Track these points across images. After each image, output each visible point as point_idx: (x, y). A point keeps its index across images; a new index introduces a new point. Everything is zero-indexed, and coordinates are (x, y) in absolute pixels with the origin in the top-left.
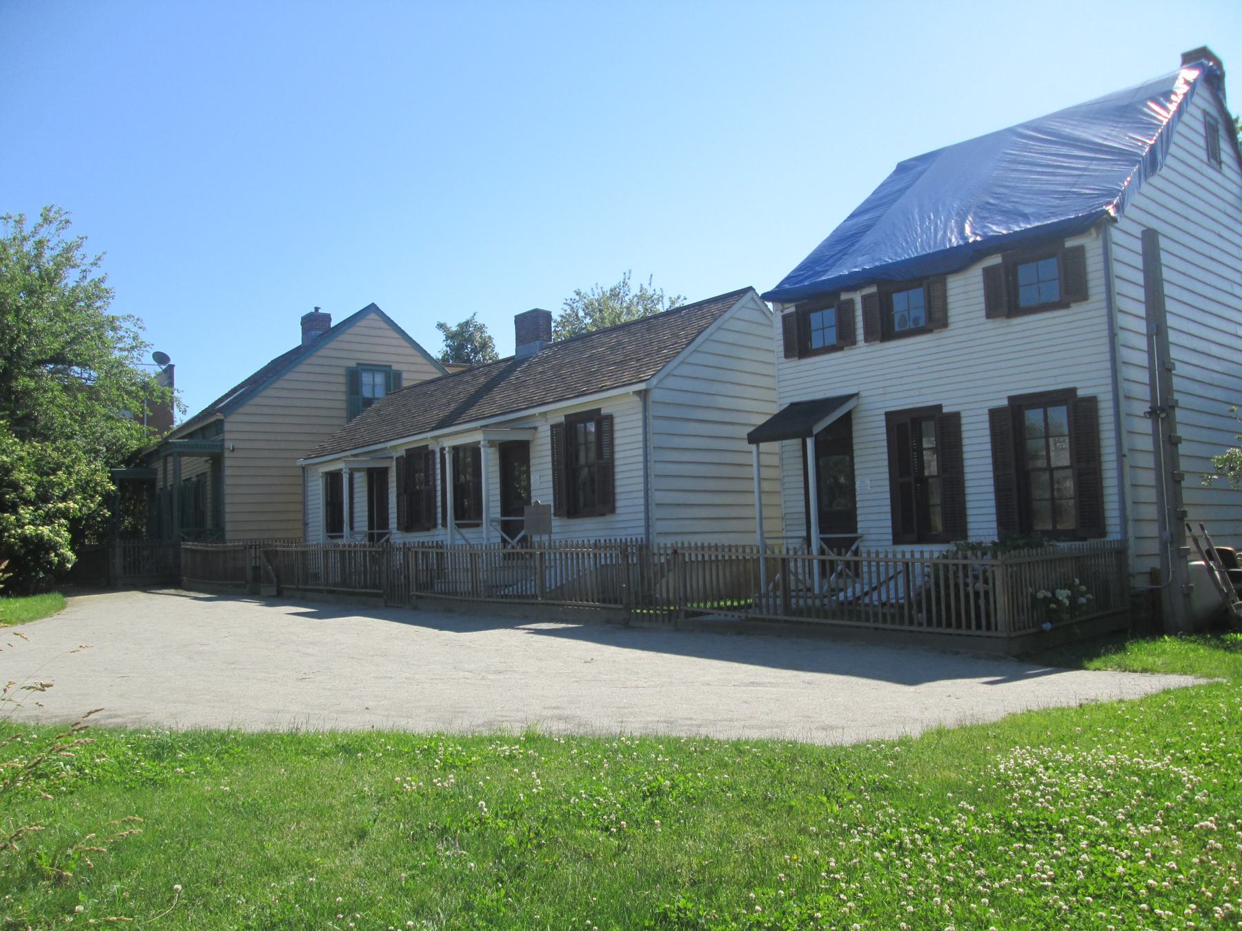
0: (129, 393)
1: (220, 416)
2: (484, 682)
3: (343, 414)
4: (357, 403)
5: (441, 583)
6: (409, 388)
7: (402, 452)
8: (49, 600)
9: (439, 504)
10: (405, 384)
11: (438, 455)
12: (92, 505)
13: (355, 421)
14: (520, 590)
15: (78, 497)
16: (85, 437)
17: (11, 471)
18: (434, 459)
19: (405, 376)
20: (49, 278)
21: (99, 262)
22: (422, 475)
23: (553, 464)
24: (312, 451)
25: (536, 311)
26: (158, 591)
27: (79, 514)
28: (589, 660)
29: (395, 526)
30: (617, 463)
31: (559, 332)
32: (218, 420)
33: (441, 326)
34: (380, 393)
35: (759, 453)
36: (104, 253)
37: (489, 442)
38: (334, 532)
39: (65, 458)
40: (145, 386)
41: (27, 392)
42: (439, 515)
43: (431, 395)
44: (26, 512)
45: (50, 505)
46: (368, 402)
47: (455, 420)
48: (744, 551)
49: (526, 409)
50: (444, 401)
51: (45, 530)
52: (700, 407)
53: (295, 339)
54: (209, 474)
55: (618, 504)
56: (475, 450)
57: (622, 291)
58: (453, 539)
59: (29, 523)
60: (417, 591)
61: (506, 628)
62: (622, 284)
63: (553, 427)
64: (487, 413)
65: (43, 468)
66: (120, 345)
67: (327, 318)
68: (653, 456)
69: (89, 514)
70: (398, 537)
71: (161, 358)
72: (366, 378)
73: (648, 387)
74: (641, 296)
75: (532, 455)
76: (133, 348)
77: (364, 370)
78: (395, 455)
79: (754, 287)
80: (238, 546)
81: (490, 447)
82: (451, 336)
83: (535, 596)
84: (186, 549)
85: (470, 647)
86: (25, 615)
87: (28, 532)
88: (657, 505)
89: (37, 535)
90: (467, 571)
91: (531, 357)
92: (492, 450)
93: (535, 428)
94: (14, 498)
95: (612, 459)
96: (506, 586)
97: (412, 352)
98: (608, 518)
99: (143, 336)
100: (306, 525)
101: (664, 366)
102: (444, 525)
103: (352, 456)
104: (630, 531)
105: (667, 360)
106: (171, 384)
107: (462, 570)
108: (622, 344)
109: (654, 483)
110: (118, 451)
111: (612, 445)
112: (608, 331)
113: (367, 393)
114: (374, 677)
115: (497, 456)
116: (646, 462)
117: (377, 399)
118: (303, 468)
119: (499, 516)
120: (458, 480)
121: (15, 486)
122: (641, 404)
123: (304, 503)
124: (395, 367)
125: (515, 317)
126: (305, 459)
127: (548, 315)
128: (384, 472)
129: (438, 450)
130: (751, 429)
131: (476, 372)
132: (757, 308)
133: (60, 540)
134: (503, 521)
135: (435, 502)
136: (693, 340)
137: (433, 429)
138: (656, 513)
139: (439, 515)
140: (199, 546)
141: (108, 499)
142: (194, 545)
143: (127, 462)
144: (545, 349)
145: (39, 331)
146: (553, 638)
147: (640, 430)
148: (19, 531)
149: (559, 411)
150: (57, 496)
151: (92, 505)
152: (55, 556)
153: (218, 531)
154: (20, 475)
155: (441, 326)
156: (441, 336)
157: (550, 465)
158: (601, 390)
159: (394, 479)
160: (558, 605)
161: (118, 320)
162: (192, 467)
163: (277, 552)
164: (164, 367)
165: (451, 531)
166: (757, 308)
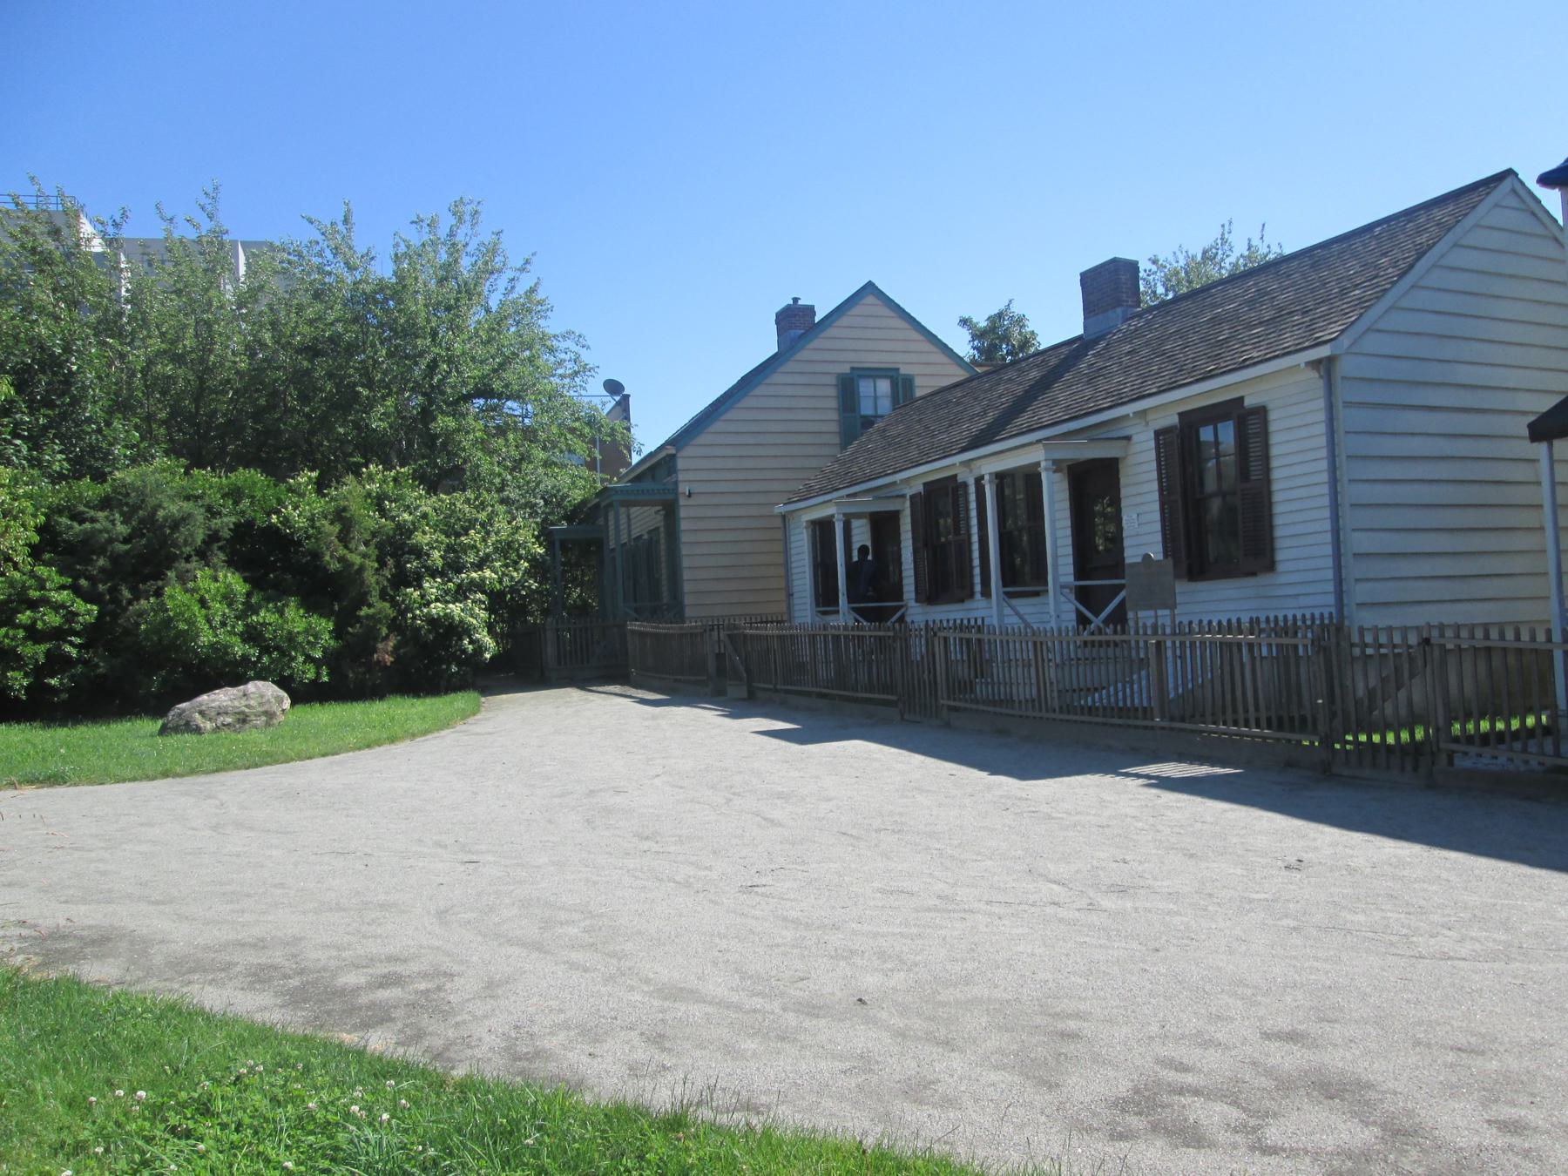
0: (572, 430)
1: (672, 450)
2: (1094, 918)
3: (836, 440)
4: (854, 424)
5: (987, 684)
6: (921, 398)
7: (918, 487)
8: (460, 700)
9: (976, 562)
10: (919, 393)
11: (972, 489)
12: (515, 574)
13: (850, 450)
14: (1112, 699)
15: (498, 564)
16: (519, 487)
17: (412, 532)
18: (966, 494)
19: (918, 382)
20: (469, 291)
21: (528, 267)
22: (949, 521)
23: (1161, 494)
24: (794, 492)
25: (1114, 261)
26: (600, 689)
27: (498, 586)
28: (1292, 860)
29: (913, 595)
30: (1275, 487)
31: (1154, 287)
32: (668, 455)
33: (965, 322)
34: (885, 406)
35: (1552, 461)
36: (534, 254)
37: (1055, 462)
38: (829, 605)
39: (478, 512)
40: (591, 422)
41: (449, 435)
42: (977, 579)
43: (958, 404)
44: (431, 587)
45: (463, 575)
46: (868, 422)
47: (998, 433)
48: (1458, 636)
49: (1110, 408)
50: (978, 409)
51: (455, 609)
52: (1426, 384)
53: (767, 345)
54: (662, 529)
55: (1280, 556)
56: (1031, 478)
57: (1220, 252)
58: (1001, 616)
59: (437, 600)
60: (949, 698)
61: (1106, 772)
62: (1219, 241)
63: (1158, 434)
64: (1046, 420)
65: (453, 527)
66: (560, 371)
67: (810, 310)
68: (1344, 474)
69: (512, 586)
70: (917, 613)
71: (613, 387)
72: (865, 388)
73: (1338, 352)
74: (1249, 257)
75: (1123, 481)
76: (576, 373)
77: (860, 377)
78: (909, 492)
79: (1516, 169)
80: (696, 627)
81: (1055, 472)
82: (978, 335)
83: (1147, 713)
84: (633, 632)
85: (1049, 817)
86: (417, 726)
87: (434, 611)
88: (1356, 555)
89: (446, 614)
90: (1030, 666)
91: (1110, 333)
92: (1058, 476)
93: (1128, 438)
94: (417, 567)
95: (1267, 480)
96: (1088, 690)
97: (927, 346)
98: (1263, 579)
99: (586, 357)
100: (790, 595)
101: (1361, 315)
102: (986, 593)
103: (848, 496)
104: (1303, 601)
105: (1363, 305)
106: (627, 418)
107: (1020, 663)
108: (1267, 294)
109: (1349, 518)
110: (559, 505)
111: (1266, 458)
112: (1237, 279)
113: (866, 409)
114: (879, 890)
115: (1065, 485)
116: (1334, 482)
117: (882, 416)
118: (784, 517)
119: (1071, 579)
120: (1005, 527)
121: (418, 552)
122: (1321, 383)
123: (786, 565)
124: (904, 370)
125: (1081, 274)
126: (785, 504)
127: (1132, 267)
128: (894, 516)
129: (971, 482)
130: (1532, 418)
131: (1024, 364)
132: (1523, 207)
133: (475, 622)
134: (1076, 586)
135: (971, 560)
136: (1411, 266)
137: (964, 450)
138: (1353, 570)
139: (977, 579)
140: (648, 627)
141: (538, 568)
142: (644, 626)
143: (569, 518)
144: (1132, 318)
145: (458, 356)
146: (1198, 799)
147: (1322, 428)
148: (425, 610)
149: (1167, 408)
150: (471, 563)
151: (515, 574)
152: (470, 643)
153: (676, 609)
154: (422, 538)
155: (965, 322)
156: (965, 335)
157: (1156, 496)
158: (1243, 366)
159: (909, 527)
160: (1192, 731)
161: (550, 339)
162: (642, 520)
163: (745, 636)
164: (617, 398)
165: (998, 605)
166: (1523, 207)
